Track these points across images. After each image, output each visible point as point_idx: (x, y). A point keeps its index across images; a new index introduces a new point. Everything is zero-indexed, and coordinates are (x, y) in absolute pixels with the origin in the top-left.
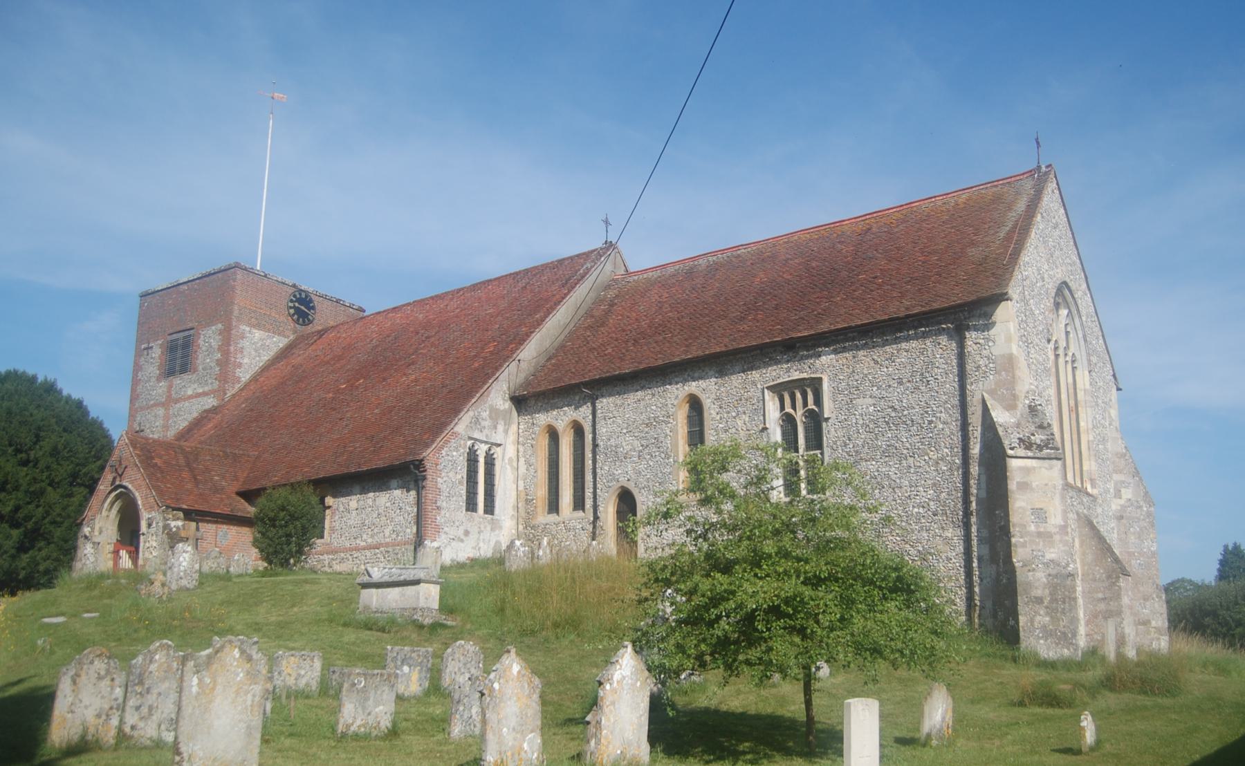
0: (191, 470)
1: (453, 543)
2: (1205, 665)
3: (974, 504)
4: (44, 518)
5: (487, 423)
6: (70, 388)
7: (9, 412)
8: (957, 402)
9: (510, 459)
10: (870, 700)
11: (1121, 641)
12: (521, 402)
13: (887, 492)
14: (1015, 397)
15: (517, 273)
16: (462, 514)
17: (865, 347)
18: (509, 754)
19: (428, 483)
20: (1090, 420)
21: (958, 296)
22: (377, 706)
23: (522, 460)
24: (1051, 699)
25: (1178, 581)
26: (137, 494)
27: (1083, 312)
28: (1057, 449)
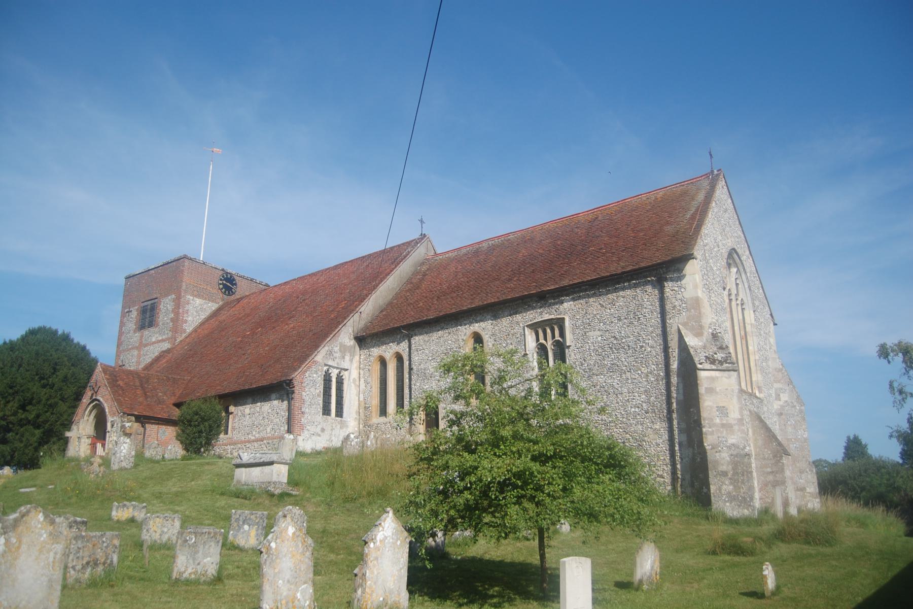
1: (314, 437)
3: (675, 404)
5: (338, 355)
6: (78, 338)
12: (362, 340)
14: (701, 327)
15: (363, 257)
16: (320, 417)
17: (594, 295)
18: (284, 602)
19: (296, 396)
22: (205, 556)
23: (362, 380)
24: (735, 549)
26: (105, 405)
27: (748, 270)
28: (734, 364)
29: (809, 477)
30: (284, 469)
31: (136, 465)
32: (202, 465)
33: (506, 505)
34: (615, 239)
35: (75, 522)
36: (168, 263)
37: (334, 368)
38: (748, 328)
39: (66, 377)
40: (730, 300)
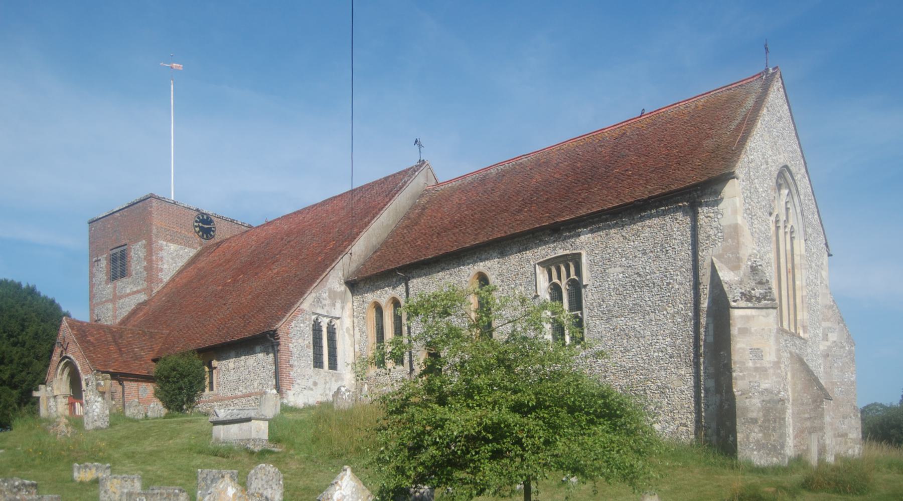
1: (305, 392)
2: (890, 466)
5: (327, 302)
6: (45, 290)
8: (690, 267)
9: (348, 329)
11: (822, 450)
14: (739, 259)
16: (310, 370)
17: (615, 226)
19: (282, 348)
20: (804, 281)
23: (357, 329)
25: (872, 404)
26: (77, 362)
27: (802, 192)
28: (773, 300)
29: (853, 422)
30: (264, 426)
31: (111, 425)
32: (183, 422)
33: (479, 460)
34: (643, 159)
35: (24, 484)
36: (134, 204)
37: (324, 316)
38: (797, 259)
39: (36, 334)
40: (778, 228)
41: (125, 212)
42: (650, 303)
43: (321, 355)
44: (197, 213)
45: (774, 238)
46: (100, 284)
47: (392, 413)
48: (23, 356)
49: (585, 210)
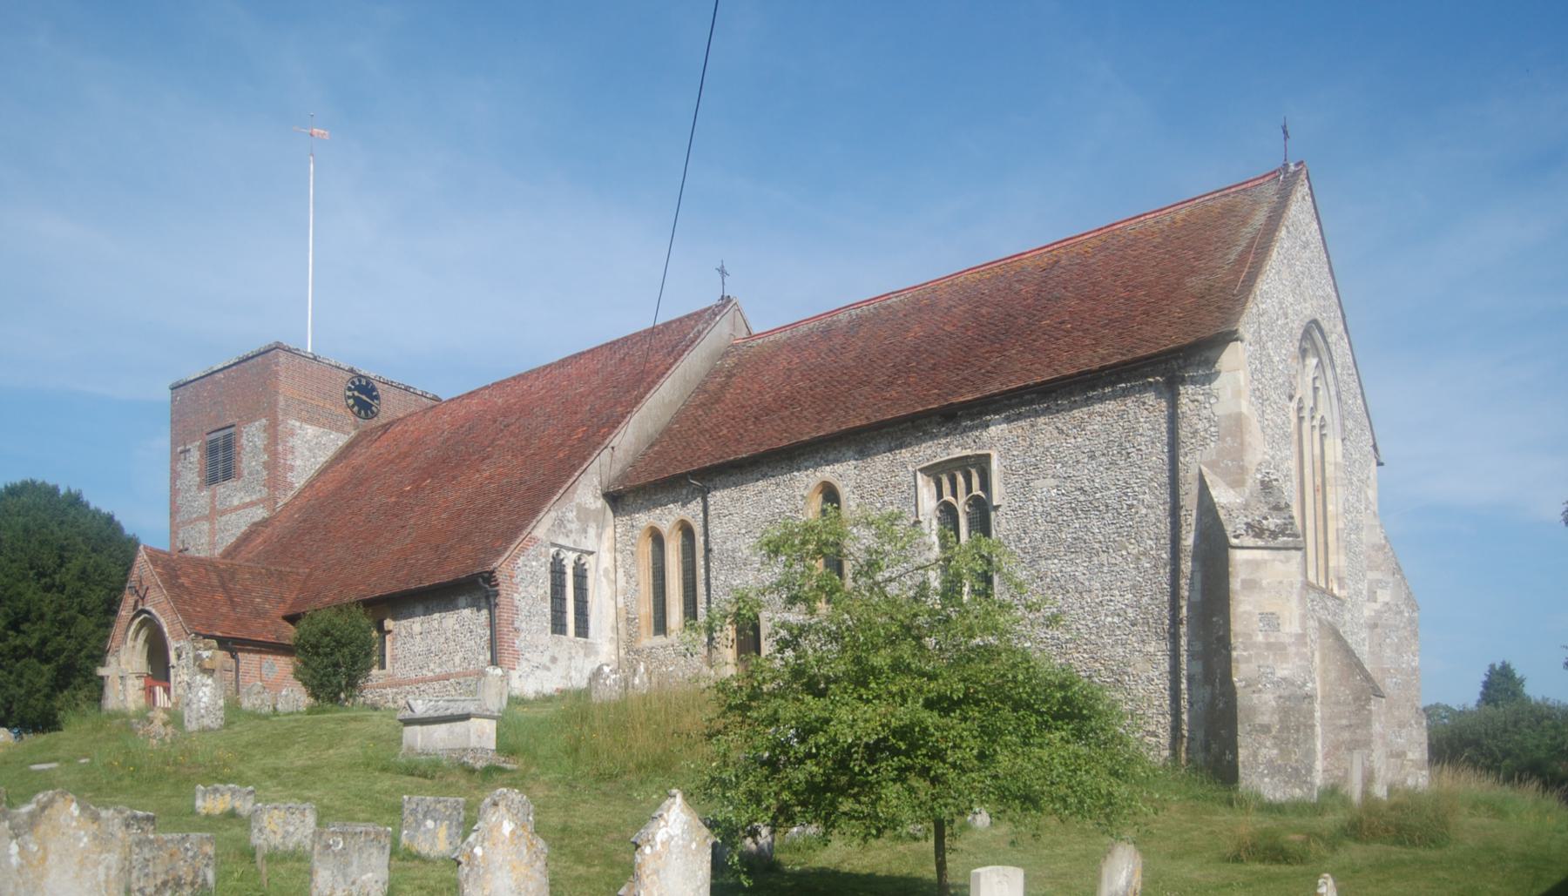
0: (226, 590)
1: (538, 672)
2: (1474, 806)
3: (1184, 611)
4: (79, 651)
5: (574, 526)
6: (99, 501)
7: (26, 530)
8: (1166, 480)
9: (606, 570)
10: (1010, 869)
13: (1073, 598)
14: (1243, 469)
15: (614, 343)
16: (547, 637)
17: (1045, 412)
19: (502, 600)
21: (1173, 338)
22: (364, 871)
23: (621, 571)
24: (1275, 853)
27: (1338, 362)
28: (1296, 536)
30: (490, 727)
31: (228, 724)
32: (344, 721)
33: (878, 783)
35: (135, 817)
36: (249, 358)
37: (569, 549)
39: (84, 571)
40: (1301, 419)
41: (232, 372)
42: (1100, 537)
43: (564, 612)
44: (350, 375)
45: (1296, 437)
46: (189, 490)
47: (730, 708)
48: (60, 608)
49: (998, 385)
